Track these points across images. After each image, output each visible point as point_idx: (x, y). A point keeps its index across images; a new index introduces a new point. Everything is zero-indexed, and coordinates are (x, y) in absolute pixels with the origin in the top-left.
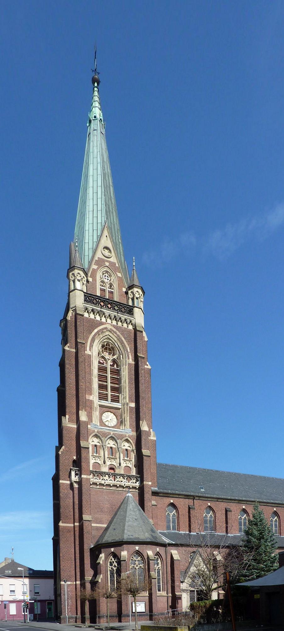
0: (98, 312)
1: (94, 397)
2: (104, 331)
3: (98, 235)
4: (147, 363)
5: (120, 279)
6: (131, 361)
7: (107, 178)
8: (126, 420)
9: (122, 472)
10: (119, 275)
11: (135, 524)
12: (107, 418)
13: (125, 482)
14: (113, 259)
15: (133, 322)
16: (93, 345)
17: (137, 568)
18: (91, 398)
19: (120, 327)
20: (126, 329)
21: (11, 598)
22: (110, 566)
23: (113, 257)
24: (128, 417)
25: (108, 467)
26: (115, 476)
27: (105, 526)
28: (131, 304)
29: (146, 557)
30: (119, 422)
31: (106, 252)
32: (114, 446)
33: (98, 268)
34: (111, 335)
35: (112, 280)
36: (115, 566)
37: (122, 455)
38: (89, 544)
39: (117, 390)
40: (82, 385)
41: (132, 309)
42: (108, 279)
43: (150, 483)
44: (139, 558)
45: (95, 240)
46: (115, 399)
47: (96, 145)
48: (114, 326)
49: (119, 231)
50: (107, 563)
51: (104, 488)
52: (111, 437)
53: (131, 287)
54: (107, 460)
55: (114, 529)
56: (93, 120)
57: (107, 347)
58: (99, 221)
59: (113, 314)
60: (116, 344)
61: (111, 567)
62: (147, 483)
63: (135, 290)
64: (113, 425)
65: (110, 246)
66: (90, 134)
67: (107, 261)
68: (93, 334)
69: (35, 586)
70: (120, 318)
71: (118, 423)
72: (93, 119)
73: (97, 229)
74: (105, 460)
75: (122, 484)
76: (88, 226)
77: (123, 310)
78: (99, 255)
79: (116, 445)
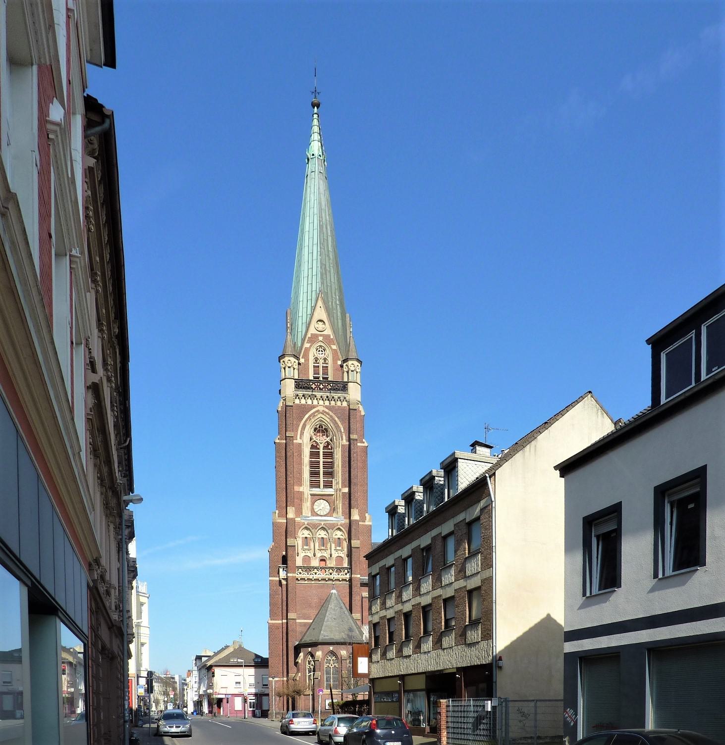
0: (309, 396)
1: (305, 489)
2: (315, 414)
3: (313, 305)
4: (364, 440)
5: (334, 352)
6: (345, 442)
7: (324, 229)
8: (338, 507)
10: (334, 347)
11: (333, 624)
12: (319, 506)
13: (335, 575)
14: (328, 331)
15: (347, 398)
17: (331, 667)
18: (301, 489)
19: (333, 406)
20: (340, 407)
21: (236, 692)
24: (341, 505)
25: (318, 559)
27: (311, 621)
29: (339, 657)
30: (332, 509)
31: (320, 326)
32: (325, 537)
33: (311, 346)
34: (323, 416)
35: (326, 354)
37: (333, 545)
38: (292, 644)
39: (329, 474)
41: (347, 385)
44: (334, 658)
45: (309, 312)
46: (328, 485)
47: (313, 192)
48: (326, 407)
49: (337, 291)
50: (306, 662)
51: (313, 582)
52: (322, 527)
53: (345, 361)
55: (314, 629)
57: (321, 429)
58: (314, 289)
59: (325, 395)
60: (329, 425)
62: (356, 576)
63: (350, 362)
64: (325, 514)
66: (307, 176)
67: (321, 335)
68: (304, 420)
69: (263, 676)
70: (333, 397)
71: (330, 510)
72: (312, 157)
73: (312, 299)
75: (331, 577)
76: (302, 297)
78: (312, 331)
79: (327, 535)
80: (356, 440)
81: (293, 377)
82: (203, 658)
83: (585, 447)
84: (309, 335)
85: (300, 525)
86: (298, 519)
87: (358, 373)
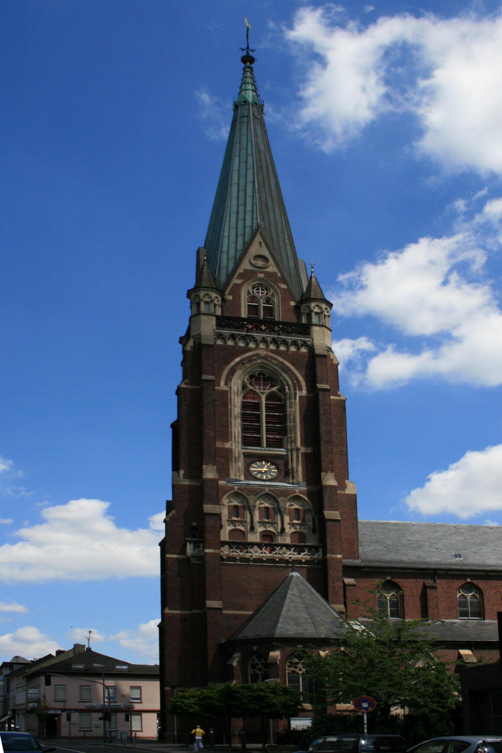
2: (253, 358)
3: (246, 240)
9: (288, 541)
16: (231, 379)
17: (300, 672)
18: (228, 445)
22: (251, 669)
23: (271, 266)
26: (272, 547)
28: (304, 321)
36: (260, 670)
40: (208, 433)
42: (262, 293)
43: (339, 556)
45: (240, 246)
46: (279, 444)
54: (256, 525)
56: (241, 105)
61: (252, 670)
65: (266, 253)
68: (233, 364)
69: (57, 687)
74: (254, 525)
77: (290, 329)
78: (245, 266)
80: (327, 390)
81: (213, 314)
82: (15, 666)
83: (111, 656)
84: (241, 270)
85: (225, 490)
86: (222, 483)
87: (217, 307)
